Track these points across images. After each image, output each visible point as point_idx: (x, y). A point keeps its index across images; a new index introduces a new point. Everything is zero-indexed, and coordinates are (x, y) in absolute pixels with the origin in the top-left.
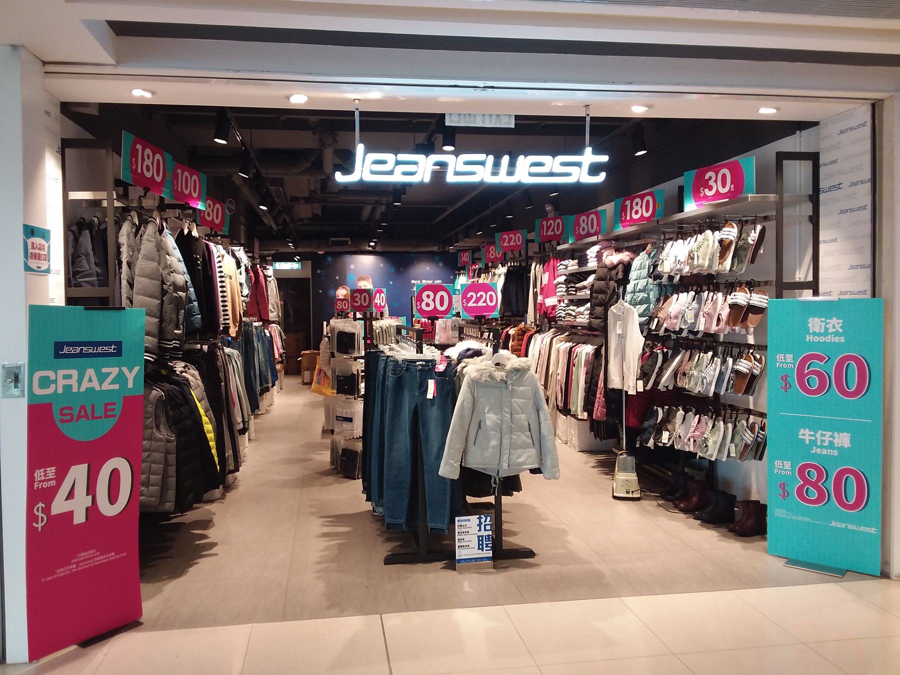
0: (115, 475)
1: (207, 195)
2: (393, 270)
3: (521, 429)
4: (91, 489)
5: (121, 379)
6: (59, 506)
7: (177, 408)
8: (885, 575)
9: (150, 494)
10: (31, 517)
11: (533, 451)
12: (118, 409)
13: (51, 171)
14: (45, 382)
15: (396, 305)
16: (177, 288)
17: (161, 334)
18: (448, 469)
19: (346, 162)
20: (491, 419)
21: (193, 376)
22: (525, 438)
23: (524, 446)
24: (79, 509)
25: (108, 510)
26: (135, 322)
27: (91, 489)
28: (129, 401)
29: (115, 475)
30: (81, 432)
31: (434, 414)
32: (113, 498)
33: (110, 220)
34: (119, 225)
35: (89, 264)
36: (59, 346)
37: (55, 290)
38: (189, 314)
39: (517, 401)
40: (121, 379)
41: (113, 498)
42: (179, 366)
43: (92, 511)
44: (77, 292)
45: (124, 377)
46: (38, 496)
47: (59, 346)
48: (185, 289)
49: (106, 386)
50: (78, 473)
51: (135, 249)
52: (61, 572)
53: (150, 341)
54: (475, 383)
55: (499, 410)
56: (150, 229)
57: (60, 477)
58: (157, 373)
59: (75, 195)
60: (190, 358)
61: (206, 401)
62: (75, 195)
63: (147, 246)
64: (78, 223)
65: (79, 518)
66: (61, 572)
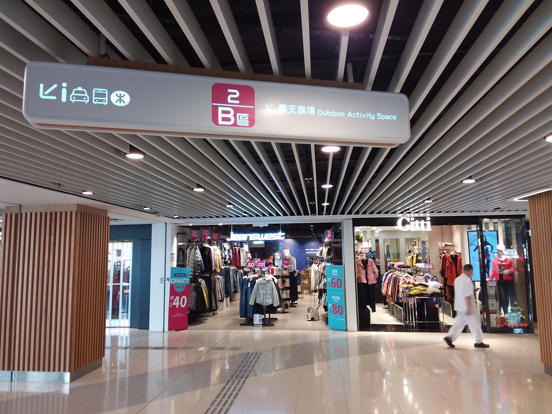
0: (184, 299)
1: (391, 40)
2: (298, 245)
3: (268, 294)
4: (179, 302)
5: (185, 281)
6: (174, 304)
7: (198, 289)
8: (346, 330)
9: (191, 306)
10: (170, 305)
11: (271, 300)
12: (185, 286)
13: (175, 240)
14: (173, 281)
15: (299, 259)
16: (198, 261)
17: (194, 272)
18: (251, 302)
19: (229, 236)
20: (261, 292)
21: (203, 282)
22: (269, 296)
23: (269, 298)
24: (177, 305)
25: (183, 306)
26: (189, 270)
27: (179, 302)
28: (187, 285)
29: (184, 299)
30: (178, 290)
31: (249, 290)
32: (183, 304)
33: (185, 249)
34: (187, 249)
35: (181, 258)
36: (175, 274)
37: (175, 266)
38: (201, 268)
39: (268, 288)
40: (185, 281)
41: (183, 304)
42: (200, 280)
43: (180, 305)
44: (179, 263)
45: (186, 281)
46: (171, 301)
47: (175, 274)
48: (201, 261)
49: (183, 282)
50: (178, 298)
51: (190, 254)
52: (174, 316)
53: (192, 273)
54: (258, 283)
55: (263, 290)
56: (193, 250)
57: (174, 298)
58: (194, 280)
59: (179, 244)
60: (203, 278)
61: (206, 289)
62: (179, 244)
63: (192, 253)
64: (180, 249)
65: (177, 307)
66: (174, 316)
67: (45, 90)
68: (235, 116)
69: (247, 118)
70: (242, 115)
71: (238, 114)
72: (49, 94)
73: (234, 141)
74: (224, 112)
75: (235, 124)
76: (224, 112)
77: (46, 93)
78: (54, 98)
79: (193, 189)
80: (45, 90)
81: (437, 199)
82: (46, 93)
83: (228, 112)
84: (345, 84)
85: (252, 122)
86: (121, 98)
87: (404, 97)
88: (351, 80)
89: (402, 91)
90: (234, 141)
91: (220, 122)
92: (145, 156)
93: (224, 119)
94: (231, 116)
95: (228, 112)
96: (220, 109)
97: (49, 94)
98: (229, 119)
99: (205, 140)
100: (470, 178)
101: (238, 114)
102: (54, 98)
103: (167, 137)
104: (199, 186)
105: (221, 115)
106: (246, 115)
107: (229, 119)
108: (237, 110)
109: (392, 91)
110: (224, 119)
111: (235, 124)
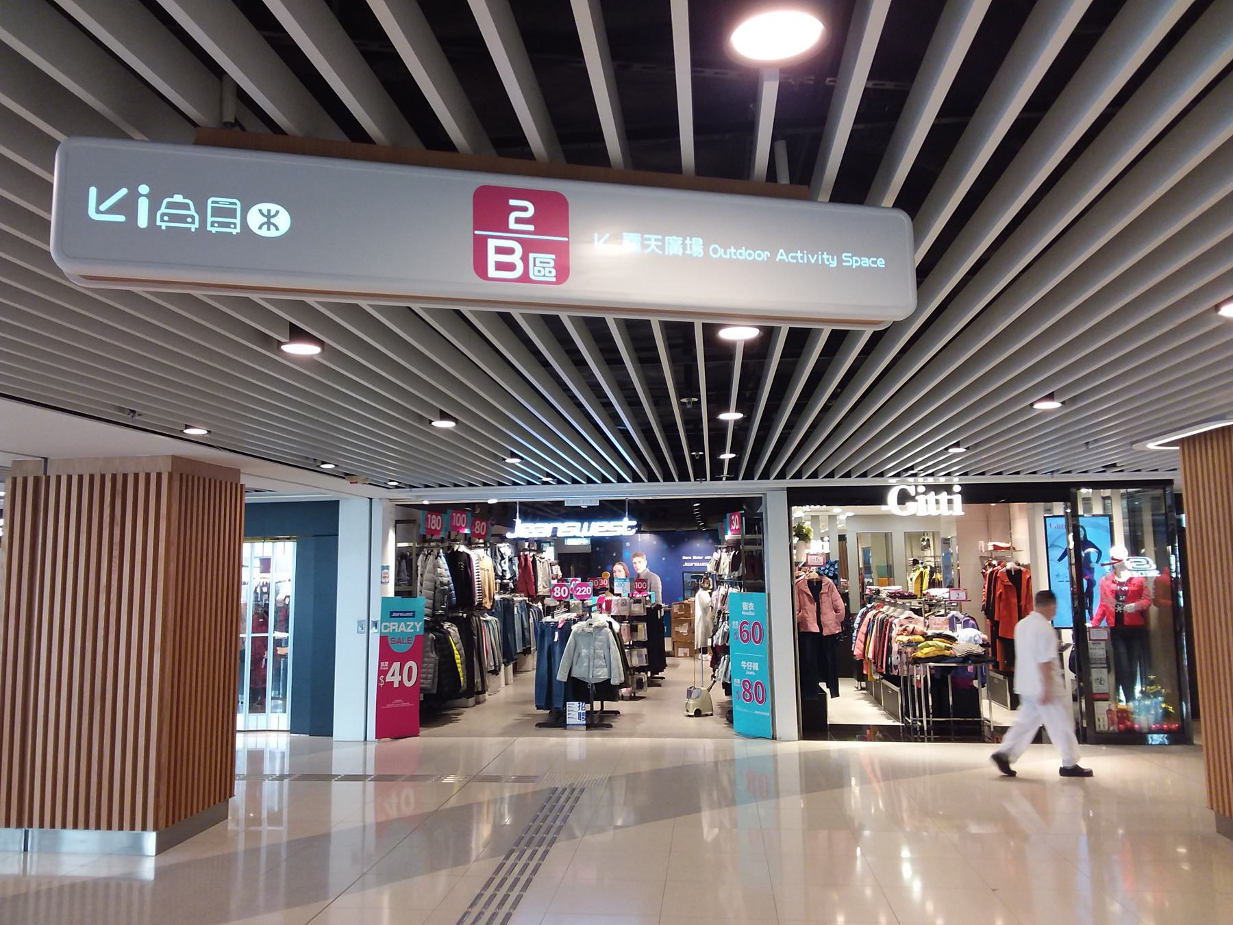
0: (410, 668)
1: (874, 90)
2: (665, 547)
3: (600, 658)
4: (401, 674)
5: (414, 627)
6: (389, 678)
7: (442, 645)
8: (774, 738)
9: (427, 684)
10: (379, 681)
11: (606, 670)
12: (413, 640)
13: (392, 535)
14: (386, 627)
15: (668, 579)
16: (442, 584)
17: (434, 608)
18: (561, 676)
19: (511, 526)
20: (584, 652)
21: (453, 630)
22: (602, 662)
23: (601, 667)
24: (396, 680)
25: (408, 684)
26: (421, 603)
27: (401, 674)
28: (417, 637)
29: (410, 668)
30: (399, 648)
31: (557, 648)
32: (409, 679)
33: (414, 556)
34: (418, 555)
35: (404, 576)
36: (392, 613)
37: (391, 593)
38: (450, 598)
39: (598, 644)
40: (414, 627)
41: (409, 679)
42: (446, 625)
43: (401, 682)
44: (400, 589)
45: (416, 627)
46: (382, 673)
47: (392, 613)
48: (448, 584)
49: (409, 630)
50: (396, 665)
51: (424, 567)
52: (389, 706)
53: (429, 611)
54: (576, 633)
55: (588, 648)
56: (431, 558)
57: (390, 667)
58: (433, 625)
59: (400, 545)
60: (454, 621)
61: (460, 645)
62: (400, 545)
63: (429, 566)
64: (401, 556)
65: (396, 685)
66: (389, 706)
67: (100, 200)
68: (525, 259)
69: (552, 264)
70: (540, 257)
71: (532, 256)
72: (110, 211)
73: (522, 315)
74: (499, 250)
75: (525, 278)
76: (499, 250)
77: (103, 207)
78: (121, 218)
79: (431, 422)
80: (100, 200)
81: (976, 445)
82: (103, 207)
83: (510, 251)
84: (770, 187)
85: (563, 272)
86: (270, 220)
87: (902, 217)
88: (784, 178)
89: (898, 204)
90: (522, 315)
91: (492, 272)
92: (323, 349)
93: (500, 266)
94: (516, 258)
95: (510, 251)
96: (492, 244)
97: (110, 211)
98: (510, 267)
99: (458, 312)
100: (1051, 397)
101: (532, 256)
102: (121, 218)
103: (372, 306)
104: (444, 416)
105: (493, 258)
106: (550, 258)
107: (510, 267)
108: (529, 247)
109: (876, 204)
110: (500, 266)
111: (525, 278)
